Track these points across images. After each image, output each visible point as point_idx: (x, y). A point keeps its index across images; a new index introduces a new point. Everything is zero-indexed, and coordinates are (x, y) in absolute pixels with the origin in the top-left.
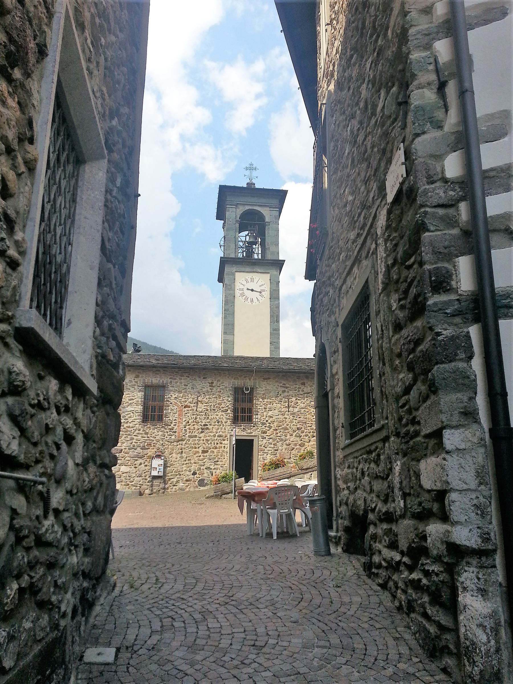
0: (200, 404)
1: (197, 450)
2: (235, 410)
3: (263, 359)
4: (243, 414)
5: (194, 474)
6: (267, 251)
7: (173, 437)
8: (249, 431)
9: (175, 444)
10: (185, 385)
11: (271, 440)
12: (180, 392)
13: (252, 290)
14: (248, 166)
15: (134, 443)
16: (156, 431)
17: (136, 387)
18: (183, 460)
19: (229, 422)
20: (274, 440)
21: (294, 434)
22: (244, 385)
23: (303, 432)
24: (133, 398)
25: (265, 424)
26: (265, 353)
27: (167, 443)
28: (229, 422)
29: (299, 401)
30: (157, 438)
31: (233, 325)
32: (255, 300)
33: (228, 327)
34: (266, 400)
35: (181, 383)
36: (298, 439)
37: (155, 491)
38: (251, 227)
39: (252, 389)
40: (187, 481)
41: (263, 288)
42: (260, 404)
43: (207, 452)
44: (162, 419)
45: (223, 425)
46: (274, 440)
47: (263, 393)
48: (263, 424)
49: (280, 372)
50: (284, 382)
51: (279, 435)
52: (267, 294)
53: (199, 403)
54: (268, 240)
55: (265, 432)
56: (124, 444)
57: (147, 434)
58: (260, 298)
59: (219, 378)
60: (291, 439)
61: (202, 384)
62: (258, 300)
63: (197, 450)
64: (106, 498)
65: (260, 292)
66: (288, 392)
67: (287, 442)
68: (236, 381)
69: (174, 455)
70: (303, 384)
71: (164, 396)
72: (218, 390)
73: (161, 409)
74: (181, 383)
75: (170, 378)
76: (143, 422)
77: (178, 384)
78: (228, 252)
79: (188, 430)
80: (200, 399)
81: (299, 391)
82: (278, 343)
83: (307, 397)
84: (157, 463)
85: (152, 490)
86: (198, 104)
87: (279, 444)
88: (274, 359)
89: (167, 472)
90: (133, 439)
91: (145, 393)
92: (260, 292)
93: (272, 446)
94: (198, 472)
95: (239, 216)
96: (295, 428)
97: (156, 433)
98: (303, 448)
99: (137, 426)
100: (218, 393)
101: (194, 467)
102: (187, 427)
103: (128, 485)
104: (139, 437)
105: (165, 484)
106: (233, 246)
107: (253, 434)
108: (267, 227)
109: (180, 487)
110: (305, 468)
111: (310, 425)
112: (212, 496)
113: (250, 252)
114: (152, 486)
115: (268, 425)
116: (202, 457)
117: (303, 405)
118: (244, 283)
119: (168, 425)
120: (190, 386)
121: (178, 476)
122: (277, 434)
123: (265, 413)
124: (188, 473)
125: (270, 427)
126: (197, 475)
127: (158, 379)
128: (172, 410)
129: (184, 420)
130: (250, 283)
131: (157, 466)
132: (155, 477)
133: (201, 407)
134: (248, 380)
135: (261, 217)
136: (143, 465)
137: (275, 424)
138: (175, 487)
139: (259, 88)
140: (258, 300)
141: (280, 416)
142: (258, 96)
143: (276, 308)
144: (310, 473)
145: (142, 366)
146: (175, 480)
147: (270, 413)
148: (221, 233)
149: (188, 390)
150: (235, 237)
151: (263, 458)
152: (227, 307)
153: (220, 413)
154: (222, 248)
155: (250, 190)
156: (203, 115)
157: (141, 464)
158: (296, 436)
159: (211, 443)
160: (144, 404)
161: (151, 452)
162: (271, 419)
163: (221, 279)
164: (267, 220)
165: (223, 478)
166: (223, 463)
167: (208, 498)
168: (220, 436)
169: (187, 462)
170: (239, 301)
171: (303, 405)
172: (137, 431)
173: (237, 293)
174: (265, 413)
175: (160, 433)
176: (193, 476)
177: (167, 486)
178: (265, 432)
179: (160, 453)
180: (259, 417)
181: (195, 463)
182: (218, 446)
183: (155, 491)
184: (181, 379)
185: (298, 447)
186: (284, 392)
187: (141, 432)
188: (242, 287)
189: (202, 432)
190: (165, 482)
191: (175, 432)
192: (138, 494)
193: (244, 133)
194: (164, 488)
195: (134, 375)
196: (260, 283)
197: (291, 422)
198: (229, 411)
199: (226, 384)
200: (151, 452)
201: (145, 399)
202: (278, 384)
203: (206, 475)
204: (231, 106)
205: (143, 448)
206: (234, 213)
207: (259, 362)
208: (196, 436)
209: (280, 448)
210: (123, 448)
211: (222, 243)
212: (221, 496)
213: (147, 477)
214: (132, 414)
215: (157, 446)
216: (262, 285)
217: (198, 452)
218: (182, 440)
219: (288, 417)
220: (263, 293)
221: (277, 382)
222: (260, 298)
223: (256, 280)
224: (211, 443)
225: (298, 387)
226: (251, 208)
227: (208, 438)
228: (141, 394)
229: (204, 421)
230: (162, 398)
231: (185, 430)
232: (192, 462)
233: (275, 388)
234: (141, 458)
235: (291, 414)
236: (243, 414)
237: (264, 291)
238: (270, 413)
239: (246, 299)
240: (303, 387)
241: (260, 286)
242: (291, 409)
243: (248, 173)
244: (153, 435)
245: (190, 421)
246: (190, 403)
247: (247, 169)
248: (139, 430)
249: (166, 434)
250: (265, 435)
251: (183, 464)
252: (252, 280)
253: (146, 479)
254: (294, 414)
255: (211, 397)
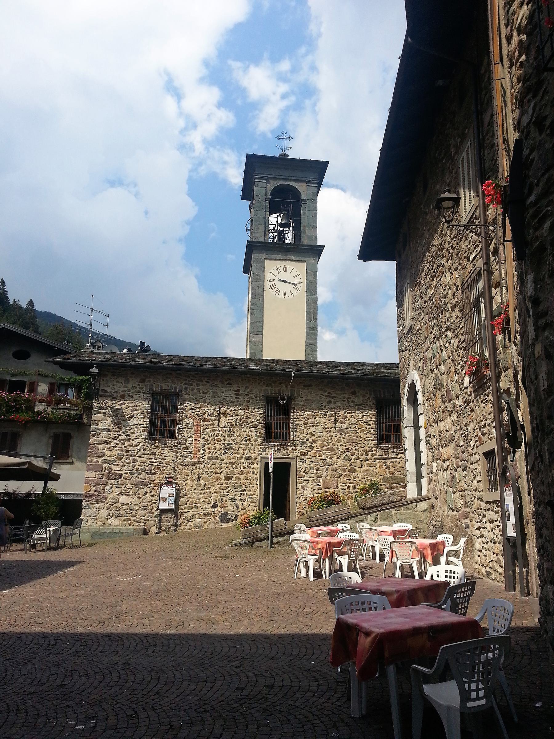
0: (223, 418)
1: (218, 475)
2: (267, 426)
3: (300, 362)
5: (215, 506)
6: (304, 235)
7: (188, 459)
8: (285, 452)
9: (191, 467)
10: (204, 393)
11: (313, 464)
13: (285, 282)
14: (281, 135)
15: (137, 467)
16: (166, 450)
17: (141, 395)
18: (200, 488)
19: (259, 441)
21: (343, 457)
23: (353, 454)
25: (305, 443)
26: (302, 357)
27: (179, 466)
28: (259, 441)
30: (168, 459)
31: (262, 322)
32: (288, 293)
33: (256, 326)
35: (199, 390)
36: (347, 463)
37: (163, 528)
38: (283, 206)
39: (289, 399)
40: (205, 515)
41: (297, 279)
42: (299, 417)
43: (231, 478)
44: (174, 435)
45: (252, 444)
47: (302, 403)
48: (303, 443)
51: (323, 457)
52: (302, 287)
54: (304, 221)
55: (305, 454)
56: (125, 468)
58: (294, 291)
59: (248, 385)
60: (339, 463)
62: (292, 293)
63: (218, 475)
65: (295, 284)
66: (335, 403)
67: (333, 467)
68: (269, 389)
69: (189, 482)
70: (354, 393)
71: (176, 407)
72: (246, 400)
73: (173, 423)
74: (199, 390)
75: (185, 384)
76: (149, 439)
77: (195, 391)
78: (256, 235)
79: (207, 451)
80: (223, 410)
81: (348, 402)
83: (358, 410)
84: (166, 492)
85: (160, 528)
86: (220, 105)
88: (312, 362)
90: (137, 461)
91: (152, 403)
92: (295, 284)
93: (315, 471)
94: (219, 504)
96: (343, 449)
97: (166, 453)
98: (353, 475)
99: (142, 444)
100: (245, 404)
101: (214, 498)
102: (206, 446)
103: (130, 520)
105: (177, 519)
106: (262, 228)
107: (290, 456)
110: (368, 506)
111: (362, 445)
113: (281, 235)
115: (309, 444)
116: (224, 485)
117: (353, 420)
118: (276, 272)
119: (181, 443)
120: (210, 394)
121: (194, 509)
122: (320, 456)
123: (305, 430)
124: (207, 505)
125: (312, 448)
126: (219, 508)
127: (170, 384)
129: (202, 437)
131: (166, 496)
132: (164, 511)
133: (224, 421)
134: (284, 388)
135: (296, 194)
136: (148, 495)
137: (318, 443)
138: (189, 524)
139: (284, 88)
140: (292, 293)
141: (324, 434)
142: (284, 96)
143: (313, 303)
144: (375, 514)
146: (190, 514)
147: (312, 430)
148: (248, 215)
149: (208, 399)
151: (302, 487)
152: (255, 301)
153: (248, 430)
154: (249, 232)
155: (283, 163)
156: (225, 117)
157: (146, 493)
158: (344, 459)
159: (236, 467)
160: (152, 415)
161: (159, 478)
162: (313, 438)
163: (247, 270)
164: (303, 197)
165: (256, 518)
166: (252, 493)
167: (235, 545)
168: (247, 458)
170: (269, 294)
171: (353, 420)
172: (142, 451)
173: (267, 285)
175: (172, 454)
176: (212, 510)
177: (179, 522)
178: (305, 454)
179: (171, 480)
180: (298, 434)
181: (216, 493)
183: (163, 528)
184: (198, 385)
185: (347, 473)
186: (329, 402)
187: (147, 452)
188: (272, 277)
190: (177, 518)
191: (191, 453)
192: (141, 533)
193: (269, 135)
194: (176, 525)
195: (139, 380)
196: (294, 273)
197: (339, 441)
198: (259, 427)
199: (256, 392)
200: (159, 478)
201: (152, 409)
202: (321, 392)
203: (229, 508)
204: (255, 107)
205: (150, 473)
206: (263, 190)
208: (217, 458)
209: (324, 474)
210: (123, 472)
211: (249, 226)
212: (253, 544)
213: (154, 511)
214: (135, 429)
215: (167, 470)
216: (297, 275)
217: (220, 478)
218: (200, 463)
219: (334, 434)
220: (298, 285)
221: (320, 390)
222: (294, 291)
223: (289, 270)
224: (236, 467)
225: (347, 396)
228: (147, 404)
229: (227, 439)
232: (212, 491)
233: (318, 398)
234: (146, 485)
235: (338, 431)
237: (299, 282)
238: (312, 430)
239: (278, 292)
240: (353, 397)
241: (295, 277)
242: (338, 425)
243: (280, 142)
244: (163, 456)
245: (210, 439)
247: (279, 138)
248: (145, 450)
250: (305, 458)
251: (201, 494)
252: (285, 269)
253: (153, 513)
254: (342, 431)
255: (236, 408)
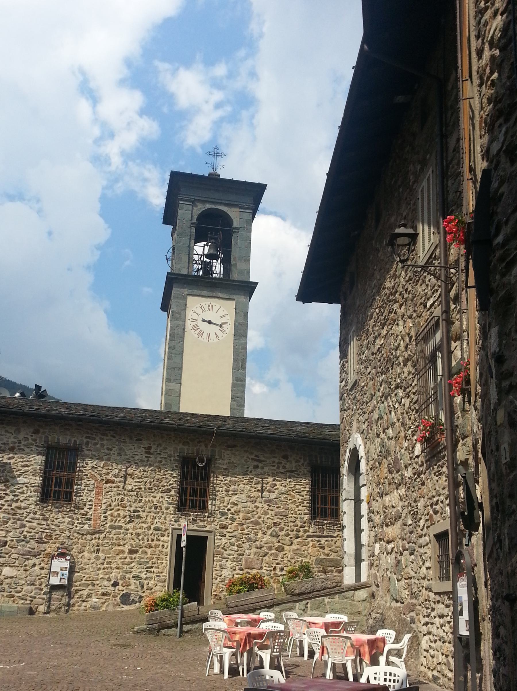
0: (129, 480)
1: (121, 548)
2: (182, 492)
4: (193, 496)
5: (115, 584)
6: (234, 269)
7: (86, 527)
8: (201, 524)
9: (89, 537)
10: (108, 449)
11: (233, 540)
12: (100, 459)
13: (210, 322)
14: (212, 150)
15: (25, 533)
20: (238, 539)
22: (198, 454)
23: (281, 530)
24: (28, 463)
27: (76, 535)
28: (172, 509)
29: (278, 483)
30: (62, 526)
31: (180, 369)
32: (213, 336)
33: (174, 373)
34: (228, 479)
35: (102, 445)
36: (274, 539)
37: (53, 607)
38: (211, 234)
39: (209, 461)
40: (103, 594)
41: (224, 320)
42: (220, 483)
43: (136, 552)
44: (71, 498)
46: (238, 539)
48: (223, 514)
49: (252, 437)
50: (256, 453)
51: (246, 532)
52: (230, 329)
53: (128, 477)
54: (235, 253)
55: (225, 527)
57: (46, 519)
58: (219, 333)
61: (133, 449)
63: (121, 548)
64: (363, 318)
65: (221, 326)
67: (258, 543)
68: (186, 448)
69: (86, 554)
70: (285, 457)
71: (75, 464)
72: (158, 459)
73: (70, 483)
74: (102, 445)
75: (87, 437)
77: (98, 446)
78: (178, 266)
79: (109, 518)
80: (130, 471)
81: (278, 468)
82: (243, 398)
83: (290, 478)
84: (59, 565)
85: (49, 607)
86: (143, 112)
87: (246, 546)
88: (237, 419)
89: (74, 579)
90: (25, 526)
92: (221, 326)
93: (235, 548)
94: (121, 582)
95: (195, 217)
96: (270, 522)
97: (61, 519)
98: (281, 554)
101: (114, 575)
102: (109, 512)
104: (35, 524)
105: (70, 598)
106: (185, 258)
107: (207, 529)
108: (234, 235)
109: (93, 604)
110: (297, 592)
111: (293, 519)
112: (145, 630)
114: (50, 599)
118: (199, 311)
119: (78, 508)
120: (115, 451)
121: (90, 587)
122: (243, 530)
123: (226, 498)
124: (106, 583)
125: (233, 520)
126: (120, 587)
127: (68, 437)
128: (87, 485)
130: (207, 314)
131: (58, 570)
132: (54, 588)
133: (131, 484)
134: (203, 447)
135: (227, 220)
136: (37, 568)
137: (241, 515)
138: (84, 604)
141: (249, 504)
142: (218, 106)
143: (242, 348)
144: (305, 602)
145: (44, 416)
146: (85, 592)
147: (234, 499)
148: (169, 243)
149: (113, 457)
150: (189, 246)
152: (173, 344)
153: (159, 495)
154: (170, 262)
155: (213, 183)
156: (148, 127)
157: (34, 565)
158: (271, 535)
159: (143, 539)
160: (45, 473)
161: (51, 547)
162: (235, 508)
163: (165, 306)
164: (235, 224)
165: (163, 601)
167: (137, 632)
169: (105, 566)
171: (283, 489)
172: (32, 515)
173: (189, 325)
174: (226, 498)
175: (67, 520)
177: (72, 602)
178: (225, 527)
179: (65, 551)
180: (218, 503)
181: (118, 568)
182: (153, 544)
184: (102, 439)
185: (273, 551)
186: (256, 467)
187: (37, 516)
188: (195, 316)
189: (130, 522)
190: (70, 596)
191: (90, 519)
192: (27, 612)
193: (199, 150)
194: (68, 605)
195: (32, 430)
196: (221, 313)
197: (265, 513)
198: (172, 492)
199: (170, 450)
200: (51, 547)
201: (46, 466)
203: (132, 587)
205: (40, 541)
206: (188, 213)
207: (219, 422)
208: (120, 527)
209: (247, 552)
210: (9, 539)
211: (170, 255)
212: (159, 631)
214: (25, 488)
215: (61, 539)
216: (224, 316)
218: (100, 532)
219: (260, 505)
221: (246, 451)
222: (219, 333)
223: (215, 309)
224: (143, 539)
225: (277, 461)
226: (213, 207)
227: (139, 531)
228: (40, 459)
229: (134, 505)
230: (73, 468)
231: (106, 517)
232: (113, 565)
233: (243, 461)
234: (35, 556)
235: (266, 502)
236: (193, 496)
237: (226, 324)
238: (234, 499)
239: (201, 334)
240: (284, 462)
241: (221, 317)
242: (265, 494)
243: (210, 159)
244: (56, 522)
245: (113, 504)
246: (115, 476)
248: (35, 513)
249: (76, 522)
250: (224, 531)
251: (99, 569)
252: (210, 308)
254: (270, 501)
